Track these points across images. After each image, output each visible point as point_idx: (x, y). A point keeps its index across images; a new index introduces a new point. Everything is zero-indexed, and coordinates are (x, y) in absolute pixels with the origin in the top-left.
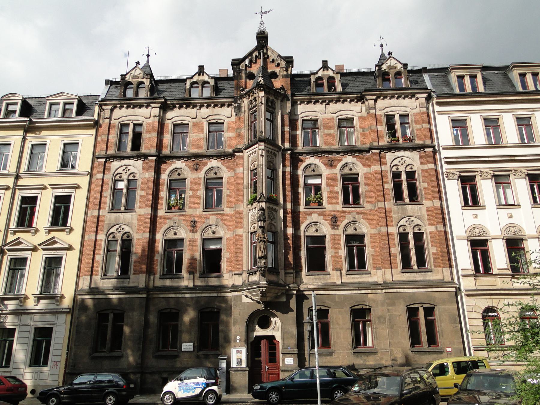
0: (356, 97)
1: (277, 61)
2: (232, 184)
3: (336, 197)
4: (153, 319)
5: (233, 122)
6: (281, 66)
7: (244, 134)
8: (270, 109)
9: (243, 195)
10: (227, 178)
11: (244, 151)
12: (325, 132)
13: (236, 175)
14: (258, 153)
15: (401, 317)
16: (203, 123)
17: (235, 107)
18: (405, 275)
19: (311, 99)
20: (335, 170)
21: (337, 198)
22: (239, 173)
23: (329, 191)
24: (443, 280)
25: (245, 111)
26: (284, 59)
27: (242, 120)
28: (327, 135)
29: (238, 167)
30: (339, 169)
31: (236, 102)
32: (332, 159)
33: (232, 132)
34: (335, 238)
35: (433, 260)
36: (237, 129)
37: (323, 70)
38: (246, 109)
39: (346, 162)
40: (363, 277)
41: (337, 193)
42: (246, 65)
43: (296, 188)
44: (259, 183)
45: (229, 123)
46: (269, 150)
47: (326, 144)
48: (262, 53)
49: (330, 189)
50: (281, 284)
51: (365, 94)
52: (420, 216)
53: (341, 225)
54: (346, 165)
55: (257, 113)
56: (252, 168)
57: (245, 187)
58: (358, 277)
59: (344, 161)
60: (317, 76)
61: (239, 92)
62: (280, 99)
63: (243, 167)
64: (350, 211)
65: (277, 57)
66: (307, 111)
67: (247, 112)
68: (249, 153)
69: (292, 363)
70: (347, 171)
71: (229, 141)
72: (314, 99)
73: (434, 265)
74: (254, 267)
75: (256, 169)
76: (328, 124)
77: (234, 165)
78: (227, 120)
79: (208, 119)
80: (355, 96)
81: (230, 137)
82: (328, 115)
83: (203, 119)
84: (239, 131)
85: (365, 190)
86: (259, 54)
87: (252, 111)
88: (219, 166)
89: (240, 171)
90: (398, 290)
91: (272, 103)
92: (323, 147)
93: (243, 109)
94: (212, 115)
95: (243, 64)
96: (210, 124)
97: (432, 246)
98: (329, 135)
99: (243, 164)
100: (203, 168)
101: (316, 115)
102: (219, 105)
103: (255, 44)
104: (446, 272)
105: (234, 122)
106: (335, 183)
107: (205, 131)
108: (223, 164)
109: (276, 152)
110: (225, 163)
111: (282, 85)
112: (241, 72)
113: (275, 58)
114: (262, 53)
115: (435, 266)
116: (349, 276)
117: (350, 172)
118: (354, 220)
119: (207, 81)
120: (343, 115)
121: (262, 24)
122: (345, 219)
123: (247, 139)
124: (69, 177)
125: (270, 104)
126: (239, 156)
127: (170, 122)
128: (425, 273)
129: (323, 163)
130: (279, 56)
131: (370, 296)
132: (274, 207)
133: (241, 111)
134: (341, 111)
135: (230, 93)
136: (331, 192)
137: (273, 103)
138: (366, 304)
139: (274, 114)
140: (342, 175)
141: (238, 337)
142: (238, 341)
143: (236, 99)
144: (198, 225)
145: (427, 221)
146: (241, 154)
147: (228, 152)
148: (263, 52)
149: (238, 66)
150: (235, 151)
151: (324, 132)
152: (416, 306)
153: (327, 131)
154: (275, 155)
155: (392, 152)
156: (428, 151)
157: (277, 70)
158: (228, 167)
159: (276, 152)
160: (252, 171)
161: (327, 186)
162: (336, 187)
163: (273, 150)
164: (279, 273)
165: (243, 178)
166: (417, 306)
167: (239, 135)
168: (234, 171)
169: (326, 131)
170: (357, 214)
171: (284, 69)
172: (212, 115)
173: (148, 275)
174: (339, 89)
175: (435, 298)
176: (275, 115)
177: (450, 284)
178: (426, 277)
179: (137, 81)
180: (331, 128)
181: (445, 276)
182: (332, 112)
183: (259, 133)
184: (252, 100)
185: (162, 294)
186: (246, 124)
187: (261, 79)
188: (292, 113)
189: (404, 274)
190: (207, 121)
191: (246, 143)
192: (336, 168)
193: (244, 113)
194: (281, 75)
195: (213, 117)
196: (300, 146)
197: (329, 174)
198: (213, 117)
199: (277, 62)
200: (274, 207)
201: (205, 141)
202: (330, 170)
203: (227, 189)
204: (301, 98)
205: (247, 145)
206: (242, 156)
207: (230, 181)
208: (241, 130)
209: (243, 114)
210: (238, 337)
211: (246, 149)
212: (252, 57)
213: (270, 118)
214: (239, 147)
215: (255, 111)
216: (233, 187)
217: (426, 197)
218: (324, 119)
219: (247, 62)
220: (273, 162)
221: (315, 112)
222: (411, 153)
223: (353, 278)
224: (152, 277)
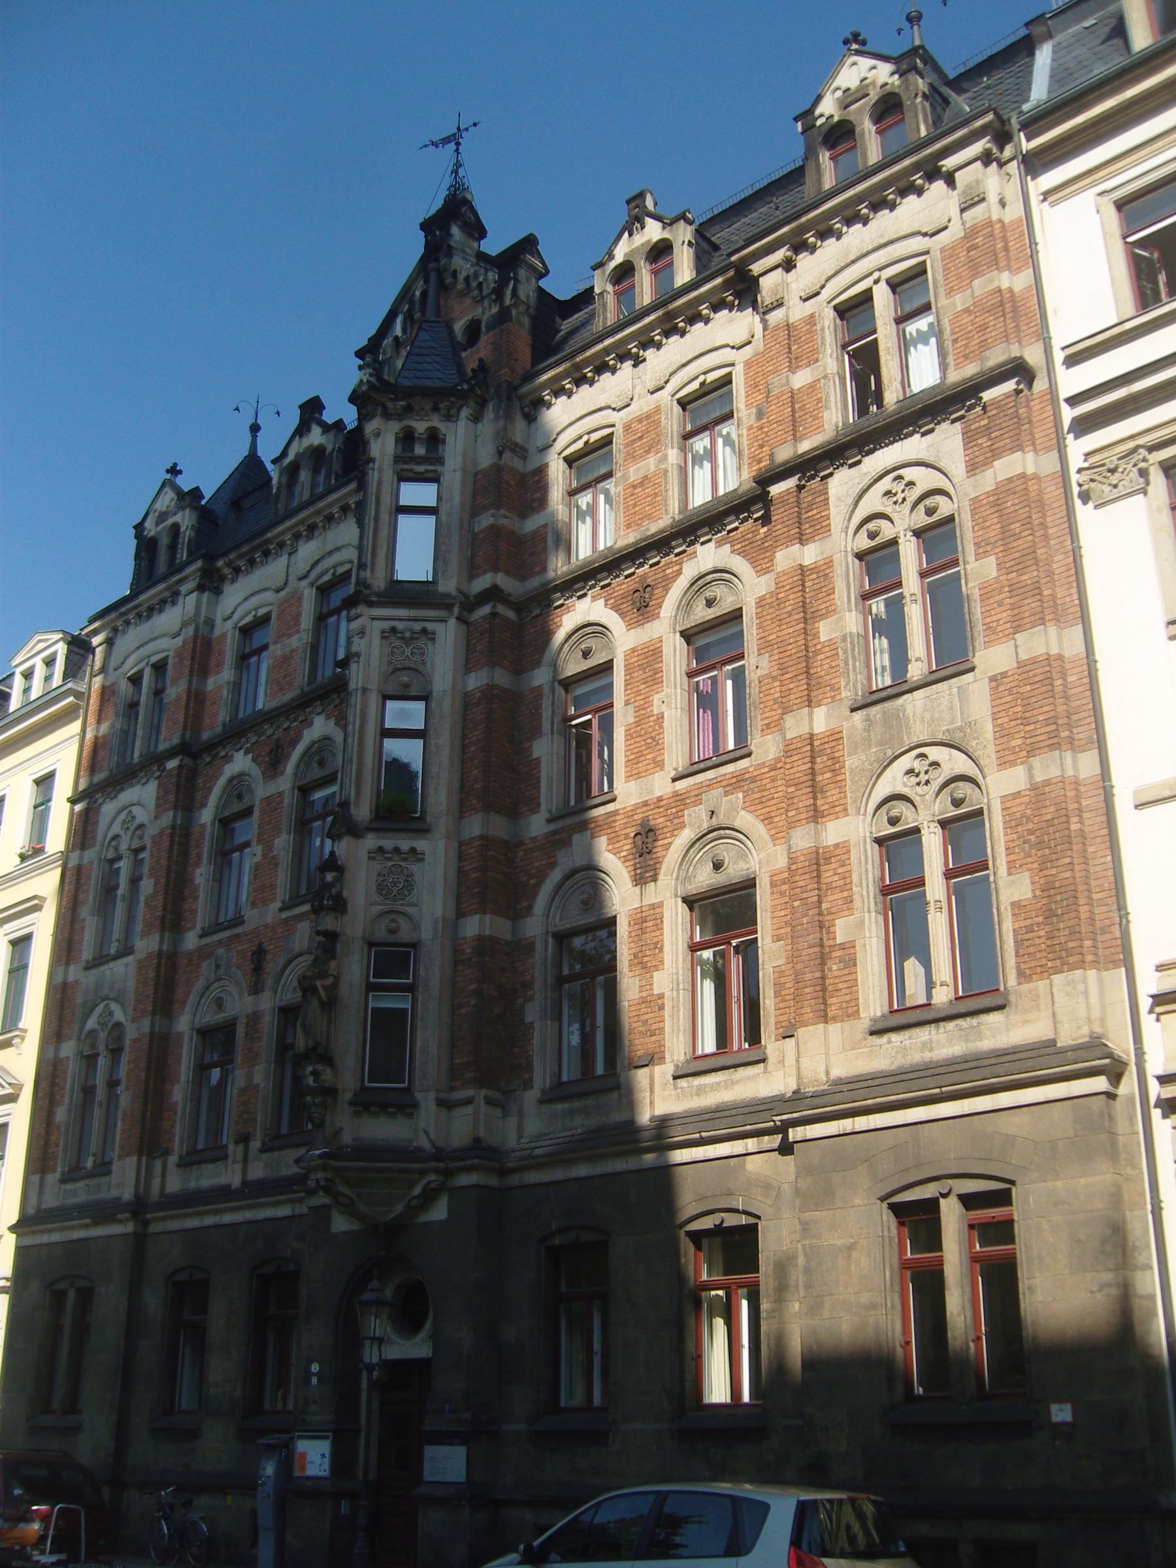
0: (726, 285)
3: (653, 738)
4: (153, 1303)
15: (855, 1254)
18: (889, 1042)
19: (578, 367)
21: (658, 744)
24: (1053, 1042)
28: (634, 487)
34: (644, 920)
35: (1016, 941)
37: (630, 235)
40: (738, 1082)
42: (396, 338)
46: (393, 630)
50: (420, 1149)
51: (742, 259)
52: (961, 729)
53: (667, 860)
54: (701, 582)
58: (718, 1084)
59: (690, 570)
60: (613, 264)
62: (465, 413)
64: (700, 786)
69: (1054, 1408)
72: (587, 362)
73: (1018, 965)
76: (641, 438)
79: (312, 576)
80: (719, 280)
85: (760, 672)
90: (846, 1125)
97: (1010, 874)
104: (1068, 994)
109: (430, 626)
115: (1021, 974)
116: (683, 1083)
118: (714, 822)
120: (687, 381)
122: (682, 826)
124: (29, 881)
127: (229, 624)
128: (974, 1021)
131: (753, 1164)
132: (405, 845)
134: (684, 365)
136: (638, 723)
138: (734, 1205)
141: (315, 1367)
142: (314, 1380)
144: (271, 967)
145: (991, 749)
152: (927, 1192)
155: (851, 466)
156: (994, 402)
161: (627, 703)
163: (416, 620)
164: (415, 1105)
166: (928, 1195)
170: (726, 794)
173: (144, 1159)
175: (1010, 1140)
177: (1082, 1054)
178: (980, 1036)
179: (164, 528)
180: (648, 452)
181: (1059, 1018)
182: (651, 385)
185: (173, 1217)
189: (885, 1038)
192: (657, 616)
200: (405, 845)
202: (639, 630)
210: (315, 1367)
212: (411, 302)
217: (988, 628)
220: (421, 668)
222: (928, 437)
223: (700, 1090)
224: (158, 1165)
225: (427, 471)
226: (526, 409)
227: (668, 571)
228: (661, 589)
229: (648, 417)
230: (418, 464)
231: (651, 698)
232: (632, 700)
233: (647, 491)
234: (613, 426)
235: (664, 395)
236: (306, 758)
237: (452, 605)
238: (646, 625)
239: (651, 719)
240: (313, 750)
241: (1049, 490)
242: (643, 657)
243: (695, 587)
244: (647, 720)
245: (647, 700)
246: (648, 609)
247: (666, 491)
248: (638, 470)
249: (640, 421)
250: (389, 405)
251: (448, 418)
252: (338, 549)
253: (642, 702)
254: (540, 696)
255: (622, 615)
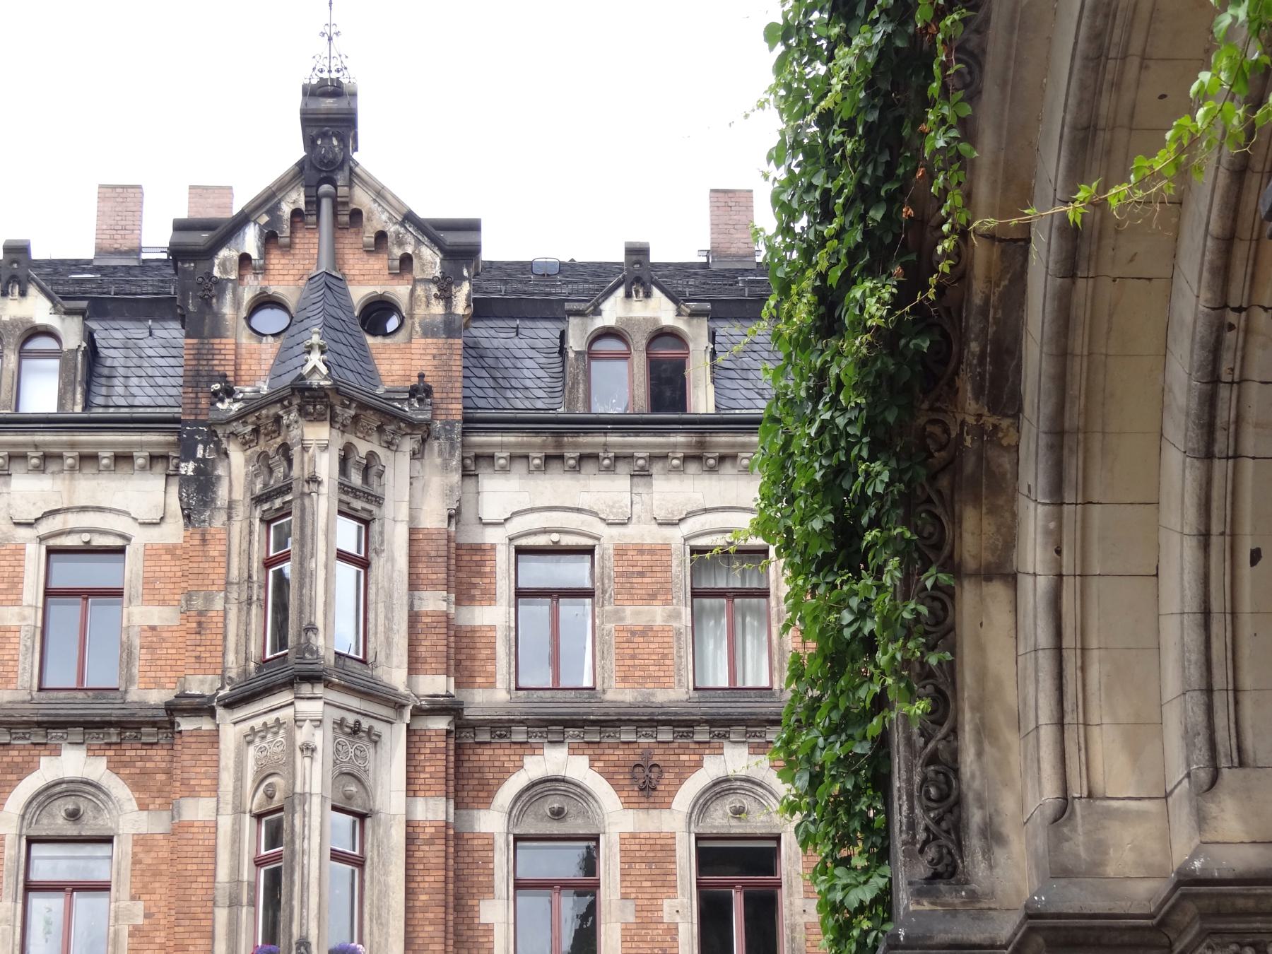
1: (401, 243)
2: (156, 874)
5: (171, 550)
6: (417, 273)
7: (225, 626)
8: (358, 504)
9: (212, 937)
10: (135, 843)
11: (220, 711)
12: (622, 619)
13: (179, 830)
14: (291, 739)
16: (19, 552)
17: (185, 481)
20: (665, 813)
22: (191, 824)
23: (632, 919)
25: (231, 506)
26: (432, 231)
27: (215, 550)
28: (633, 633)
29: (192, 793)
30: (686, 808)
31: (189, 455)
32: (655, 759)
33: (163, 603)
36: (189, 596)
37: (628, 295)
38: (238, 494)
39: (721, 774)
41: (673, 930)
42: (245, 259)
43: (470, 902)
44: (291, 891)
45: (151, 553)
47: (624, 679)
48: (326, 205)
49: (639, 910)
54: (721, 788)
55: (293, 519)
56: (255, 802)
57: (222, 898)
59: (713, 768)
61: (204, 402)
63: (215, 790)
65: (402, 224)
66: (538, 504)
67: (240, 512)
68: (245, 727)
70: (720, 820)
71: (150, 647)
74: (266, 850)
75: (280, 809)
76: (641, 574)
77: (168, 772)
78: (140, 538)
79: (45, 528)
81: (153, 628)
82: (642, 533)
83: (23, 532)
84: (198, 603)
85: (806, 918)
86: (314, 202)
87: (266, 506)
88: (93, 777)
89: (197, 810)
91: (366, 471)
92: (610, 696)
93: (222, 493)
94: (67, 510)
95: (227, 253)
96: (51, 551)
98: (643, 633)
99: (216, 779)
100: (12, 786)
101: (584, 528)
102: (106, 456)
103: (293, 150)
105: (175, 546)
106: (665, 881)
107: (32, 591)
108: (114, 767)
109: (379, 727)
110: (125, 765)
111: (421, 376)
112: (222, 292)
113: (392, 229)
114: (326, 205)
117: (737, 828)
119: (46, 326)
121: (330, 39)
123: (237, 653)
125: (356, 479)
126: (197, 733)
129: (609, 776)
130: (409, 218)
133: (213, 500)
134: (706, 511)
135: (161, 391)
137: (369, 467)
139: (375, 527)
140: (699, 838)
143: (191, 434)
146: (206, 724)
147: (143, 705)
148: (334, 198)
149: (203, 266)
150: (173, 709)
151: (618, 616)
153: (635, 615)
154: (374, 739)
157: (400, 291)
158: (138, 783)
159: (379, 727)
160: (259, 817)
161: (625, 897)
162: (666, 903)
165: (213, 851)
167: (200, 624)
168: (171, 806)
169: (629, 610)
171: (434, 290)
172: (67, 510)
174: (702, 400)
176: (382, 533)
180: (653, 596)
182: (661, 515)
183: (299, 635)
184: (271, 452)
186: (234, 573)
187: (315, 359)
188: (467, 514)
190: (41, 539)
191: (233, 673)
193: (230, 518)
194: (417, 320)
195: (74, 521)
196: (498, 685)
197: (634, 836)
198: (74, 521)
199: (398, 252)
201: (29, 643)
202: (642, 815)
203: (133, 898)
204: (510, 438)
205: (237, 680)
206: (215, 736)
207: (148, 859)
208: (209, 598)
209: (219, 520)
211: (231, 704)
212: (274, 211)
213: (353, 550)
214: (201, 685)
215: (284, 512)
216: (161, 888)
218: (621, 551)
219: (250, 241)
220: (363, 777)
221: (578, 510)
225: (364, 509)
226: (468, 462)
227: (683, 757)
228: (672, 776)
229: (652, 551)
230: (356, 497)
231: (660, 902)
232: (633, 896)
233: (651, 646)
234: (599, 539)
235: (675, 536)
236: (41, 798)
237: (403, 706)
238: (651, 812)
239: (660, 926)
240: (57, 789)
241: (277, 267)
242: (648, 848)
243: (717, 789)
244: (654, 926)
245: (655, 902)
246: (656, 793)
247: (680, 657)
248: (638, 613)
249: (641, 552)
250: (338, 409)
251: (389, 445)
252: (99, 509)
253: (645, 902)
254: (490, 846)
255: (617, 787)
